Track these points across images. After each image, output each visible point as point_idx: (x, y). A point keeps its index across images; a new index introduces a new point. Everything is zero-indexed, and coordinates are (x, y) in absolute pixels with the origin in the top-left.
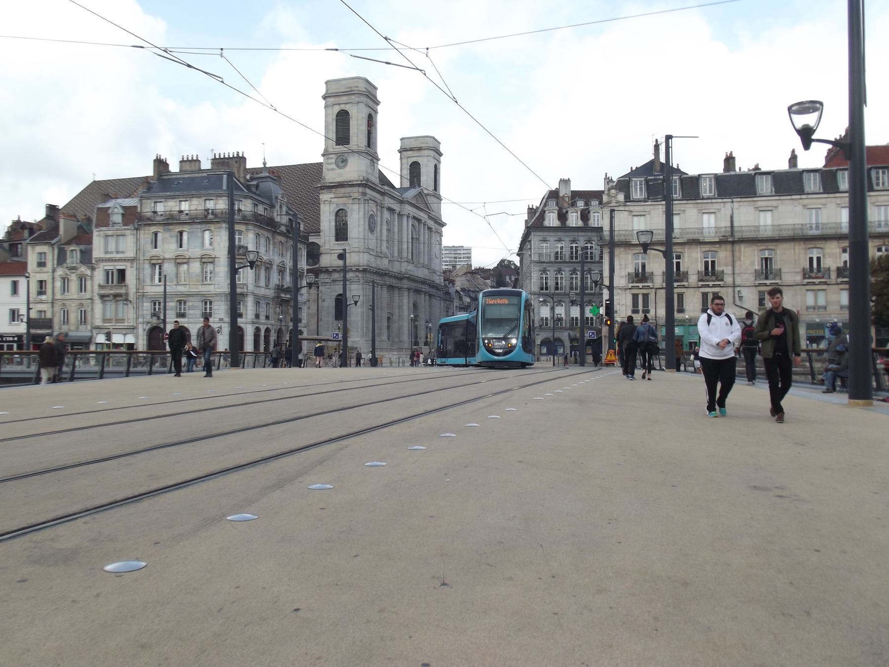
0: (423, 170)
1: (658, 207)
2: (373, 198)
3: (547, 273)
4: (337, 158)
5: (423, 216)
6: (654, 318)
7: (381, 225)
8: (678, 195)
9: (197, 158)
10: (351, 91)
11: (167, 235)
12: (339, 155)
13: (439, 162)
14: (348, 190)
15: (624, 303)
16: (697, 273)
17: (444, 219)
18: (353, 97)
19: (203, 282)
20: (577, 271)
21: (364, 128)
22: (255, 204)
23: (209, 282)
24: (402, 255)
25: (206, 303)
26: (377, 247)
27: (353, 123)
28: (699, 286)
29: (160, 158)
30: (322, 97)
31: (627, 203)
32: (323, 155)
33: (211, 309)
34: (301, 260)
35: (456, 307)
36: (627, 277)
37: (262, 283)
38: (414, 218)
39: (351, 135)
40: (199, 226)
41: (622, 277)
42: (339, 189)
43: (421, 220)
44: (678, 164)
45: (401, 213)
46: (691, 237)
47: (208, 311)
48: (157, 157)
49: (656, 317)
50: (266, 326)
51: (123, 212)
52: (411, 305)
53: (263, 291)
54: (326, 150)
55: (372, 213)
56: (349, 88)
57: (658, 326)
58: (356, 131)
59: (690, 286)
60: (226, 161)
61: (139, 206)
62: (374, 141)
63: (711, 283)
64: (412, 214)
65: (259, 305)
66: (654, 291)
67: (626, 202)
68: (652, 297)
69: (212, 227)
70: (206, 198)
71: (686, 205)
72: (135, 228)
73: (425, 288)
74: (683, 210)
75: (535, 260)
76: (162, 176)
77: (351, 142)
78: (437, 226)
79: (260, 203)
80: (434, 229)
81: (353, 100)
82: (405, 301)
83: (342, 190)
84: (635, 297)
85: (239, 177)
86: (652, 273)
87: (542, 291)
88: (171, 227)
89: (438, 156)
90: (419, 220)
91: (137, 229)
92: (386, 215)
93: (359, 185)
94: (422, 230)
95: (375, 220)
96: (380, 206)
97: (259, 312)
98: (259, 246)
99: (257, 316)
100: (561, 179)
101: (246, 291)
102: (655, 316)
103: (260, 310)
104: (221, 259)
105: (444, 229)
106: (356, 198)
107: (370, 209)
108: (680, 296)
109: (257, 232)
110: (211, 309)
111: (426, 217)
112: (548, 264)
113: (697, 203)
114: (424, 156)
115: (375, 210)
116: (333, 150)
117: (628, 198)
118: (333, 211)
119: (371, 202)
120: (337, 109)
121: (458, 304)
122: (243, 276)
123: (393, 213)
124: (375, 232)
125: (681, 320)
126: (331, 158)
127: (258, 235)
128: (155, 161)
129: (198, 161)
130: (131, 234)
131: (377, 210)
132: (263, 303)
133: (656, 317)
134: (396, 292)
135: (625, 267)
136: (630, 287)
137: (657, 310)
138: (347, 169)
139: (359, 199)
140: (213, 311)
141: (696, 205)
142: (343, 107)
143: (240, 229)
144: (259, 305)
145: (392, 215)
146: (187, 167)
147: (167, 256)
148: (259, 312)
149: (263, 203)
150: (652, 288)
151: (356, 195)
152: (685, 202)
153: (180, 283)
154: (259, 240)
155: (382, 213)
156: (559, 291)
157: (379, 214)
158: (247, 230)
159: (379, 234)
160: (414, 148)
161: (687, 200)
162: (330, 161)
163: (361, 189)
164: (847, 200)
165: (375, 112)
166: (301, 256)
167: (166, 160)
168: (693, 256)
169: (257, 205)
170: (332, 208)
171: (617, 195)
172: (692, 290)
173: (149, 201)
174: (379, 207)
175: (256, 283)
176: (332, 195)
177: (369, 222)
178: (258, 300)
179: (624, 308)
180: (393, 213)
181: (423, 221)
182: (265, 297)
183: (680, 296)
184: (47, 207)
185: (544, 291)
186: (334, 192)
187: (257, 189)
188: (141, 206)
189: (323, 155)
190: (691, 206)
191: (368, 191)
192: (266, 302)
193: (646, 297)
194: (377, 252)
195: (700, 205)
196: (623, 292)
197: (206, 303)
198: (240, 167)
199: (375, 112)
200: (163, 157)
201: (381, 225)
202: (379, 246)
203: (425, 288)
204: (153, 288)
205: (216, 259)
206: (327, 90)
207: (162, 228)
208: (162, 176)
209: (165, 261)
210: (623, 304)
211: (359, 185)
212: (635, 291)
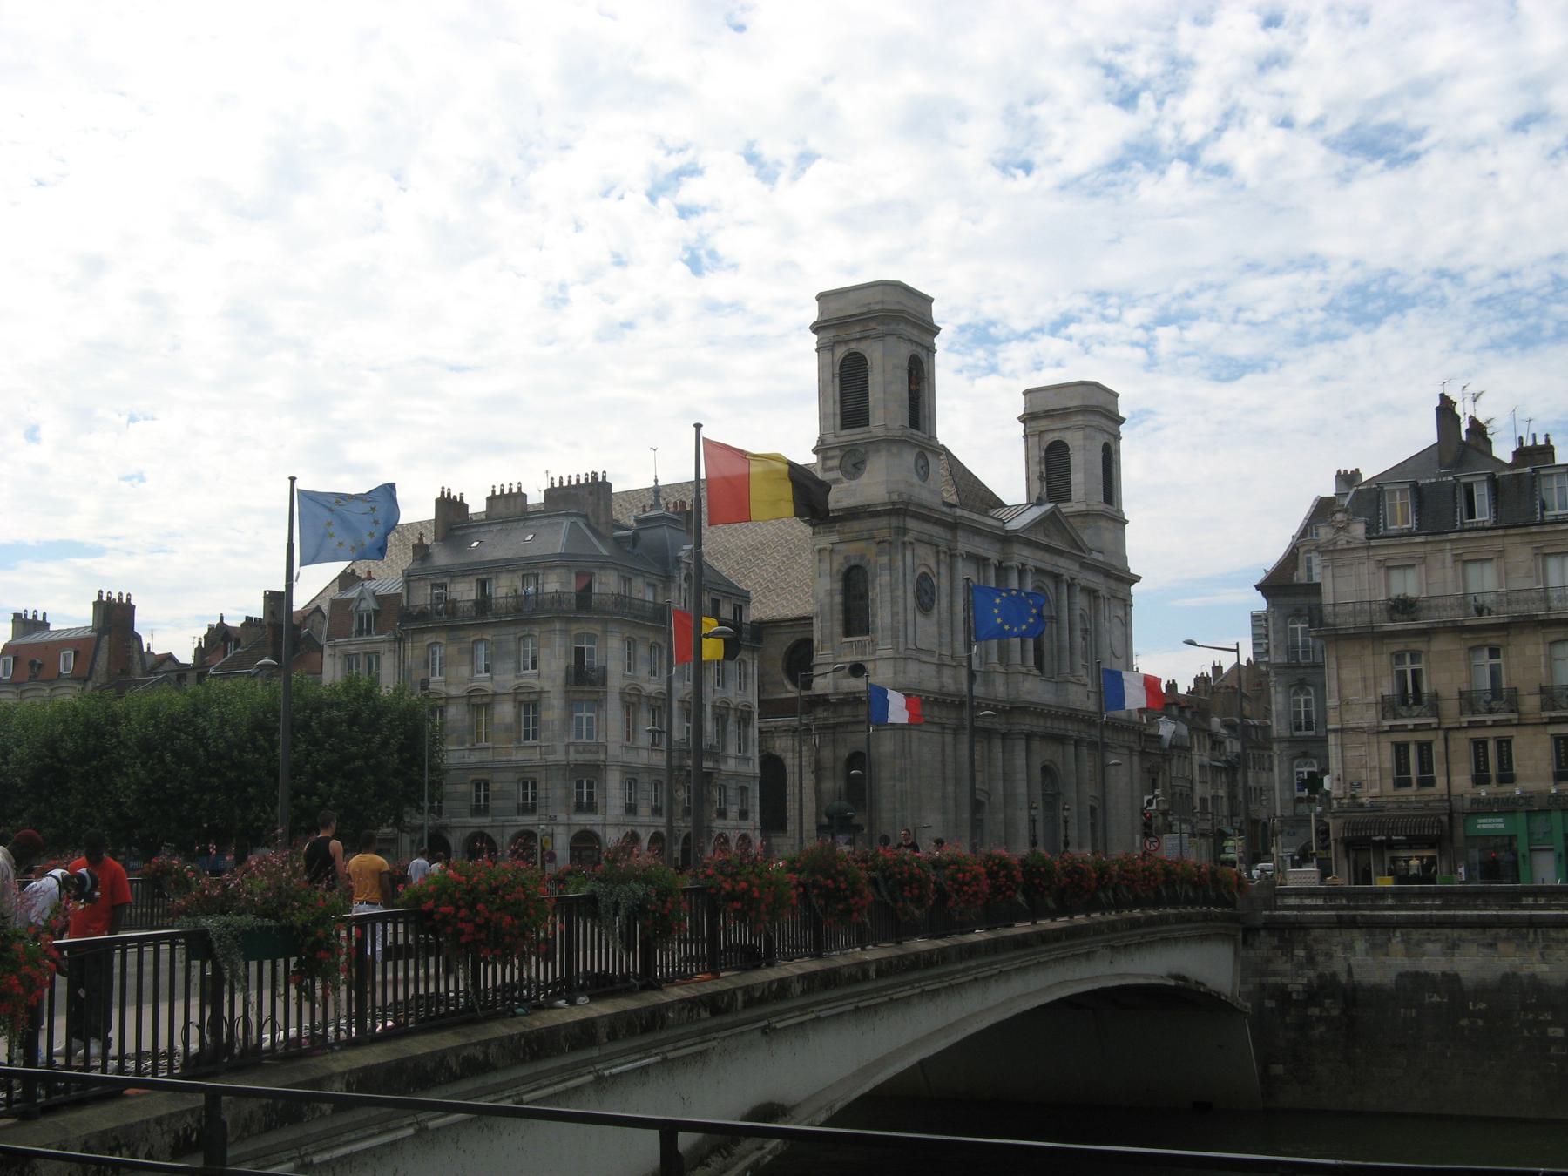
0: (1076, 459)
1: (1442, 546)
2: (926, 538)
3: (1308, 691)
4: (844, 456)
5: (1067, 567)
6: (1446, 797)
7: (952, 595)
8: (1487, 518)
9: (520, 489)
10: (869, 312)
11: (452, 650)
12: (847, 449)
13: (1117, 437)
14: (869, 523)
15: (1376, 763)
16: (1538, 689)
17: (1134, 568)
18: (873, 325)
19: (519, 742)
20: (1309, 685)
21: (901, 389)
22: (623, 577)
23: (483, 744)
24: (1008, 659)
25: (525, 787)
26: (940, 645)
27: (876, 381)
28: (1464, 725)
29: (449, 494)
30: (811, 328)
31: (1373, 543)
32: (816, 451)
33: (590, 795)
34: (745, 684)
35: (1202, 767)
36: (1380, 706)
37: (644, 739)
38: (1039, 571)
39: (871, 404)
40: (512, 630)
41: (1368, 705)
42: (848, 524)
43: (1062, 575)
44: (1547, 435)
45: (1003, 565)
46: (1520, 609)
47: (585, 800)
48: (443, 493)
49: (1449, 794)
50: (652, 830)
51: (377, 608)
52: (1037, 772)
53: (643, 758)
54: (821, 440)
55: (924, 569)
56: (865, 305)
57: (1455, 815)
58: (882, 395)
59: (1524, 722)
60: (573, 491)
61: (405, 594)
62: (927, 414)
63: (1410, 723)
64: (1031, 564)
65: (635, 786)
66: (1441, 734)
67: (1369, 539)
68: (1438, 748)
69: (536, 630)
70: (525, 572)
71: (1506, 540)
72: (396, 637)
73: (1072, 730)
74: (1500, 551)
75: (1279, 661)
76: (451, 529)
77: (871, 419)
78: (1113, 584)
79: (637, 575)
80: (1103, 592)
81: (873, 332)
82: (1020, 761)
83: (856, 526)
84: (1401, 750)
85: (598, 524)
86: (1436, 694)
87: (1297, 734)
88: (461, 634)
89: (1110, 424)
90: (1057, 578)
91: (399, 640)
92: (965, 570)
93: (888, 513)
94: (1065, 597)
95: (932, 586)
96: (945, 552)
97: (635, 800)
98: (635, 663)
99: (631, 809)
100: (1339, 471)
101: (602, 757)
102: (1446, 792)
103: (639, 797)
104: (551, 695)
105: (1134, 589)
106: (884, 541)
107: (917, 562)
108: (1504, 744)
109: (627, 635)
110: (590, 795)
111: (1076, 567)
112: (1309, 671)
113: (1529, 534)
114: (1077, 428)
115: (932, 562)
116: (836, 440)
117: (1372, 530)
118: (839, 570)
119: (917, 545)
120: (841, 352)
121: (1206, 760)
122: (598, 726)
123: (984, 565)
124: (935, 611)
125: (1508, 799)
126: (832, 458)
127: (630, 643)
128: (438, 501)
129: (521, 496)
130: (389, 651)
131: (938, 563)
132: (645, 781)
133: (1449, 794)
134: (997, 744)
135: (1375, 684)
136: (1387, 728)
137: (1452, 778)
138: (865, 478)
139: (890, 543)
140: (537, 802)
141: (1528, 538)
142: (853, 346)
143: (590, 631)
144: (635, 786)
145: (981, 571)
146: (500, 508)
147: (453, 691)
148: (635, 800)
149: (642, 573)
150: (1435, 729)
151: (883, 534)
152: (1501, 532)
153: (479, 745)
154: (635, 651)
155: (952, 568)
156: (1303, 733)
157: (944, 570)
158: (605, 632)
159: (945, 615)
160: (1053, 410)
161: (1427, 534)
162: (831, 463)
163: (894, 522)
164: (814, 659)
165: (928, 351)
166: (745, 677)
167: (461, 497)
168: (1528, 653)
169: (630, 579)
170: (836, 565)
171: (1348, 524)
172: (1529, 731)
173: (422, 583)
174: (942, 556)
175: (628, 740)
176: (835, 538)
177: (918, 590)
178: (635, 776)
179: (1376, 775)
180: (984, 565)
181: (1066, 577)
182: (649, 770)
183: (1504, 744)
184: (265, 597)
185: (1303, 733)
186: (838, 531)
187: (634, 545)
188: (408, 592)
189: (816, 451)
190: (1518, 539)
191: (911, 524)
192: (654, 778)
193: (1425, 749)
194: (940, 655)
195: (1538, 538)
196: (1374, 738)
197: (525, 787)
198: (598, 504)
199: (928, 351)
200: (455, 493)
201: (952, 595)
202: (947, 640)
203: (1072, 730)
204: (477, 753)
205: (545, 695)
206: (821, 314)
207: (444, 635)
208: (451, 529)
209: (497, 698)
210: (1375, 767)
211: (888, 513)
212: (1400, 737)
